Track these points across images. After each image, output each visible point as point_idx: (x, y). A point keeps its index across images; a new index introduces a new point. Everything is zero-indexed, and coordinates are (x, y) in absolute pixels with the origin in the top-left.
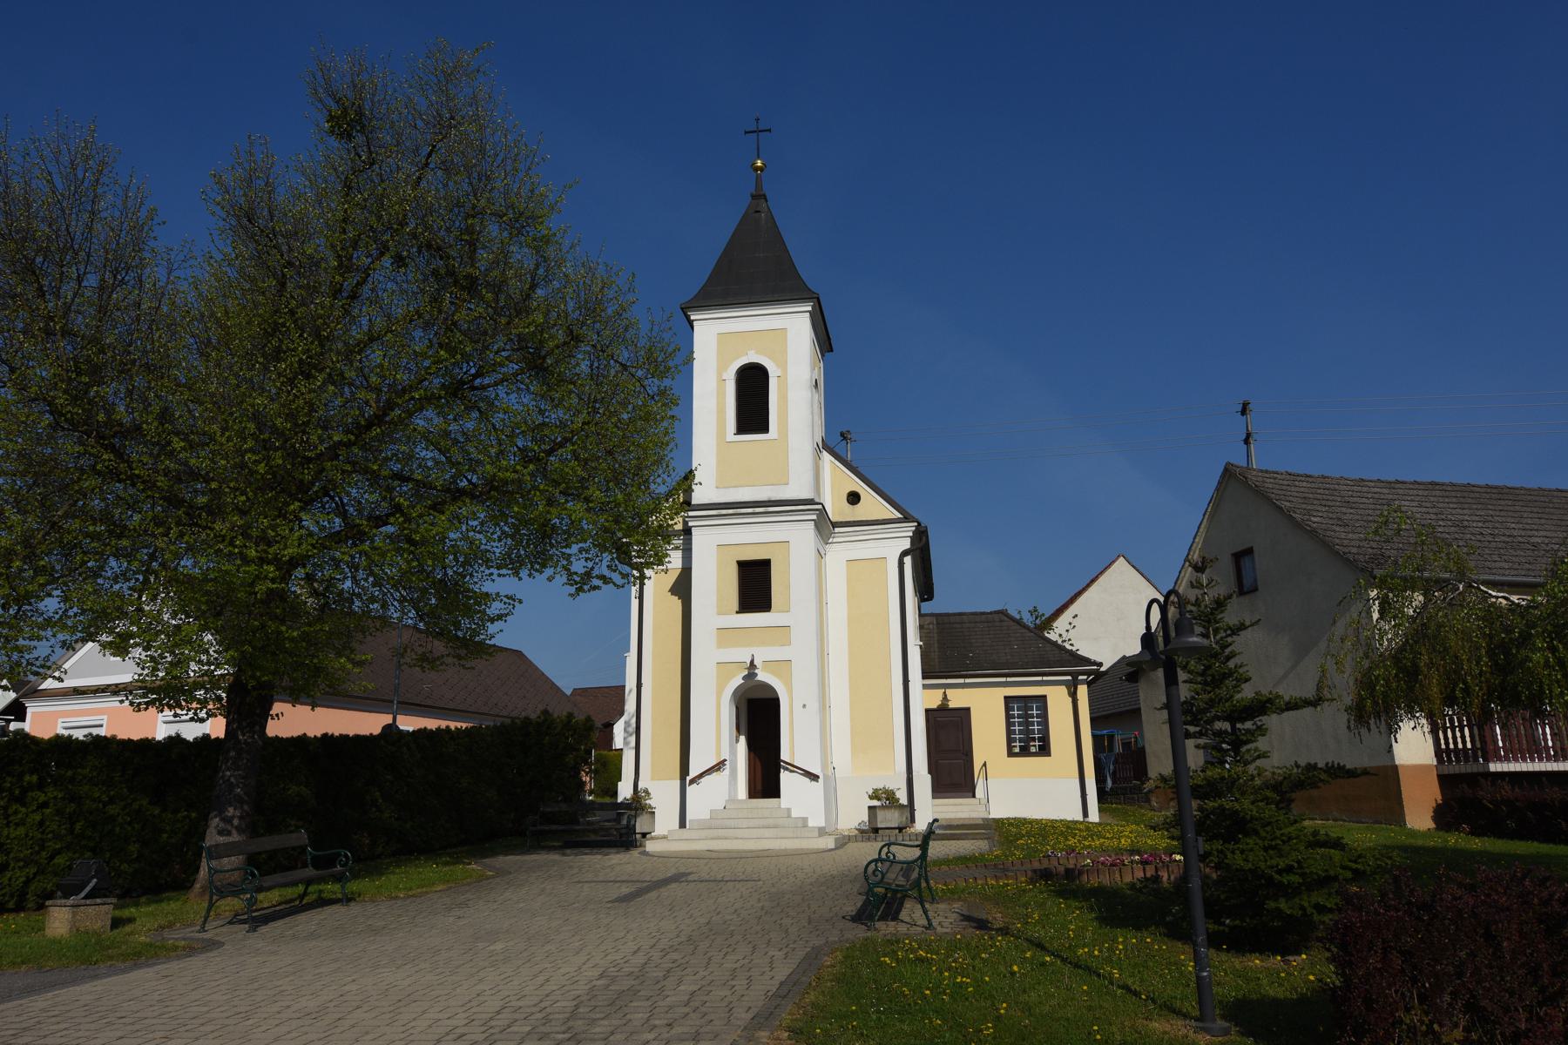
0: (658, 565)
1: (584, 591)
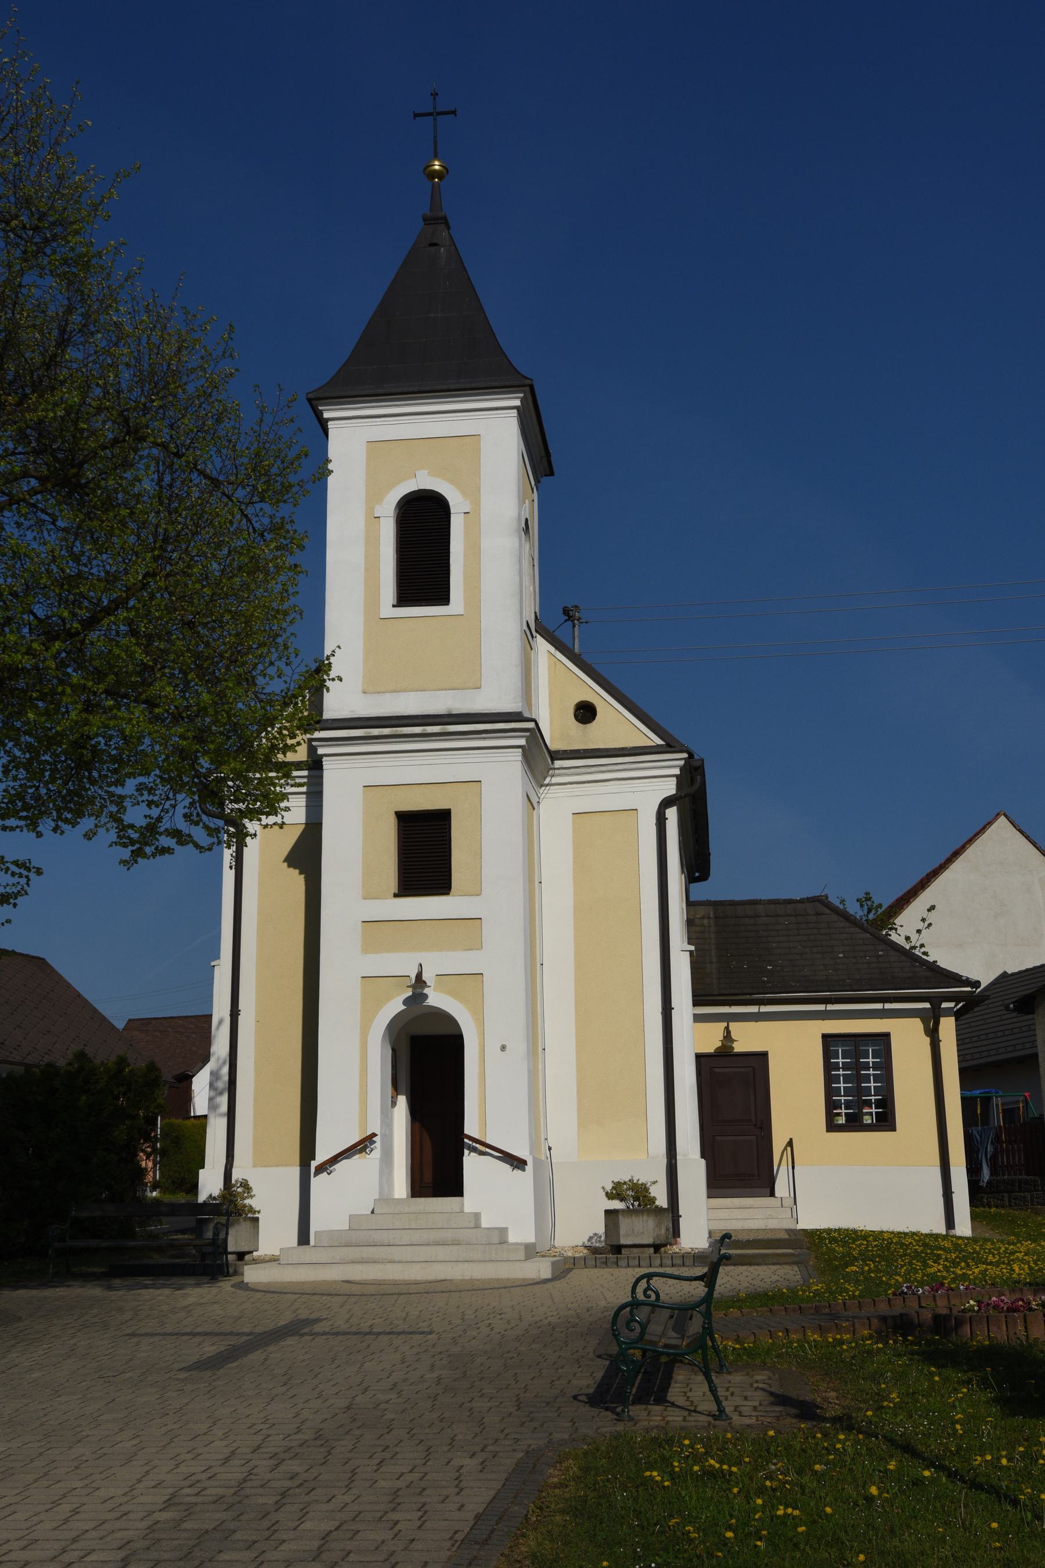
0: (268, 814)
1: (145, 856)
